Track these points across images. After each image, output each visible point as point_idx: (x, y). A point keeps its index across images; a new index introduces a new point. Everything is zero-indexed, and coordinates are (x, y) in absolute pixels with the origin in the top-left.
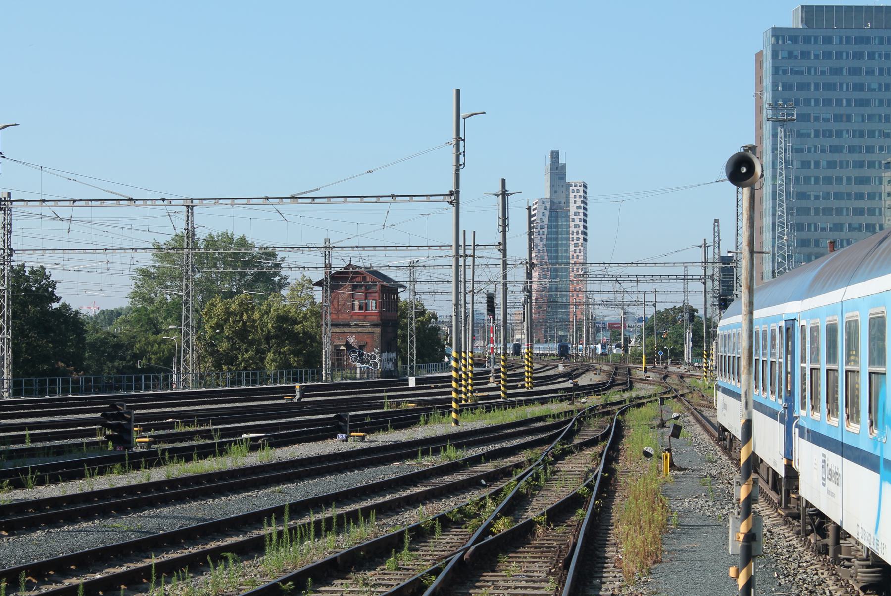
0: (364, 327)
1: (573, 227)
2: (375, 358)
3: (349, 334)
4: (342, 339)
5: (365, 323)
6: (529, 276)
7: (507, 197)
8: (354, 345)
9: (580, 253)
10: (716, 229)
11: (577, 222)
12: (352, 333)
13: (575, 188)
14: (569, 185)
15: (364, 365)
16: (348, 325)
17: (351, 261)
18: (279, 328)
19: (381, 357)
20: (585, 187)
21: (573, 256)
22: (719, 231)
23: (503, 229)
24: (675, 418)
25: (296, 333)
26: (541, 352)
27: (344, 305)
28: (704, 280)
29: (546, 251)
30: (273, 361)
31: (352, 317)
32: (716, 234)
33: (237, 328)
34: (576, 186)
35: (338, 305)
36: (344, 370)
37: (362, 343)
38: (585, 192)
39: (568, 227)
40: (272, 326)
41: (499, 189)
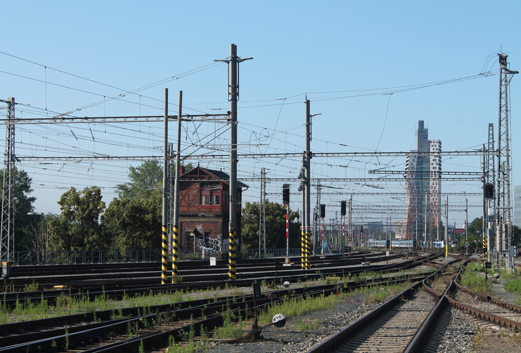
0: (209, 217)
1: (432, 168)
2: (217, 243)
3: (197, 223)
4: (191, 227)
5: (211, 215)
6: (306, 164)
7: (237, 63)
8: (201, 232)
9: (436, 185)
10: (491, 132)
11: (435, 165)
12: (199, 223)
13: (434, 144)
14: (430, 142)
15: (209, 249)
16: (197, 216)
17: (199, 164)
18: (132, 217)
19: (222, 242)
20: (440, 143)
21: (432, 187)
22: (493, 134)
23: (233, 97)
24: (276, 324)
25: (146, 221)
26: (405, 246)
27: (193, 200)
28: (483, 179)
29: (415, 183)
30: (125, 243)
31: (199, 209)
32: (491, 136)
33: (85, 215)
34: (434, 143)
35: (189, 200)
36: (193, 252)
37: (207, 231)
38: (440, 147)
39: (429, 168)
40: (126, 215)
41: (228, 55)
